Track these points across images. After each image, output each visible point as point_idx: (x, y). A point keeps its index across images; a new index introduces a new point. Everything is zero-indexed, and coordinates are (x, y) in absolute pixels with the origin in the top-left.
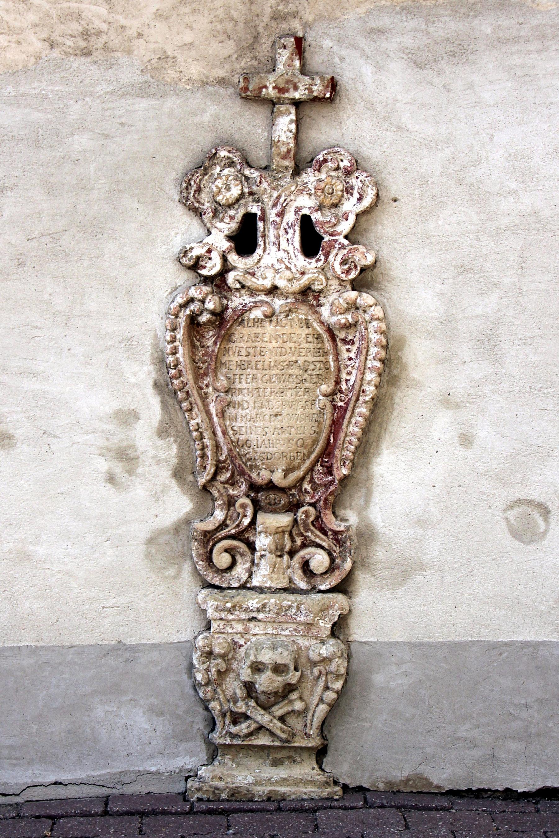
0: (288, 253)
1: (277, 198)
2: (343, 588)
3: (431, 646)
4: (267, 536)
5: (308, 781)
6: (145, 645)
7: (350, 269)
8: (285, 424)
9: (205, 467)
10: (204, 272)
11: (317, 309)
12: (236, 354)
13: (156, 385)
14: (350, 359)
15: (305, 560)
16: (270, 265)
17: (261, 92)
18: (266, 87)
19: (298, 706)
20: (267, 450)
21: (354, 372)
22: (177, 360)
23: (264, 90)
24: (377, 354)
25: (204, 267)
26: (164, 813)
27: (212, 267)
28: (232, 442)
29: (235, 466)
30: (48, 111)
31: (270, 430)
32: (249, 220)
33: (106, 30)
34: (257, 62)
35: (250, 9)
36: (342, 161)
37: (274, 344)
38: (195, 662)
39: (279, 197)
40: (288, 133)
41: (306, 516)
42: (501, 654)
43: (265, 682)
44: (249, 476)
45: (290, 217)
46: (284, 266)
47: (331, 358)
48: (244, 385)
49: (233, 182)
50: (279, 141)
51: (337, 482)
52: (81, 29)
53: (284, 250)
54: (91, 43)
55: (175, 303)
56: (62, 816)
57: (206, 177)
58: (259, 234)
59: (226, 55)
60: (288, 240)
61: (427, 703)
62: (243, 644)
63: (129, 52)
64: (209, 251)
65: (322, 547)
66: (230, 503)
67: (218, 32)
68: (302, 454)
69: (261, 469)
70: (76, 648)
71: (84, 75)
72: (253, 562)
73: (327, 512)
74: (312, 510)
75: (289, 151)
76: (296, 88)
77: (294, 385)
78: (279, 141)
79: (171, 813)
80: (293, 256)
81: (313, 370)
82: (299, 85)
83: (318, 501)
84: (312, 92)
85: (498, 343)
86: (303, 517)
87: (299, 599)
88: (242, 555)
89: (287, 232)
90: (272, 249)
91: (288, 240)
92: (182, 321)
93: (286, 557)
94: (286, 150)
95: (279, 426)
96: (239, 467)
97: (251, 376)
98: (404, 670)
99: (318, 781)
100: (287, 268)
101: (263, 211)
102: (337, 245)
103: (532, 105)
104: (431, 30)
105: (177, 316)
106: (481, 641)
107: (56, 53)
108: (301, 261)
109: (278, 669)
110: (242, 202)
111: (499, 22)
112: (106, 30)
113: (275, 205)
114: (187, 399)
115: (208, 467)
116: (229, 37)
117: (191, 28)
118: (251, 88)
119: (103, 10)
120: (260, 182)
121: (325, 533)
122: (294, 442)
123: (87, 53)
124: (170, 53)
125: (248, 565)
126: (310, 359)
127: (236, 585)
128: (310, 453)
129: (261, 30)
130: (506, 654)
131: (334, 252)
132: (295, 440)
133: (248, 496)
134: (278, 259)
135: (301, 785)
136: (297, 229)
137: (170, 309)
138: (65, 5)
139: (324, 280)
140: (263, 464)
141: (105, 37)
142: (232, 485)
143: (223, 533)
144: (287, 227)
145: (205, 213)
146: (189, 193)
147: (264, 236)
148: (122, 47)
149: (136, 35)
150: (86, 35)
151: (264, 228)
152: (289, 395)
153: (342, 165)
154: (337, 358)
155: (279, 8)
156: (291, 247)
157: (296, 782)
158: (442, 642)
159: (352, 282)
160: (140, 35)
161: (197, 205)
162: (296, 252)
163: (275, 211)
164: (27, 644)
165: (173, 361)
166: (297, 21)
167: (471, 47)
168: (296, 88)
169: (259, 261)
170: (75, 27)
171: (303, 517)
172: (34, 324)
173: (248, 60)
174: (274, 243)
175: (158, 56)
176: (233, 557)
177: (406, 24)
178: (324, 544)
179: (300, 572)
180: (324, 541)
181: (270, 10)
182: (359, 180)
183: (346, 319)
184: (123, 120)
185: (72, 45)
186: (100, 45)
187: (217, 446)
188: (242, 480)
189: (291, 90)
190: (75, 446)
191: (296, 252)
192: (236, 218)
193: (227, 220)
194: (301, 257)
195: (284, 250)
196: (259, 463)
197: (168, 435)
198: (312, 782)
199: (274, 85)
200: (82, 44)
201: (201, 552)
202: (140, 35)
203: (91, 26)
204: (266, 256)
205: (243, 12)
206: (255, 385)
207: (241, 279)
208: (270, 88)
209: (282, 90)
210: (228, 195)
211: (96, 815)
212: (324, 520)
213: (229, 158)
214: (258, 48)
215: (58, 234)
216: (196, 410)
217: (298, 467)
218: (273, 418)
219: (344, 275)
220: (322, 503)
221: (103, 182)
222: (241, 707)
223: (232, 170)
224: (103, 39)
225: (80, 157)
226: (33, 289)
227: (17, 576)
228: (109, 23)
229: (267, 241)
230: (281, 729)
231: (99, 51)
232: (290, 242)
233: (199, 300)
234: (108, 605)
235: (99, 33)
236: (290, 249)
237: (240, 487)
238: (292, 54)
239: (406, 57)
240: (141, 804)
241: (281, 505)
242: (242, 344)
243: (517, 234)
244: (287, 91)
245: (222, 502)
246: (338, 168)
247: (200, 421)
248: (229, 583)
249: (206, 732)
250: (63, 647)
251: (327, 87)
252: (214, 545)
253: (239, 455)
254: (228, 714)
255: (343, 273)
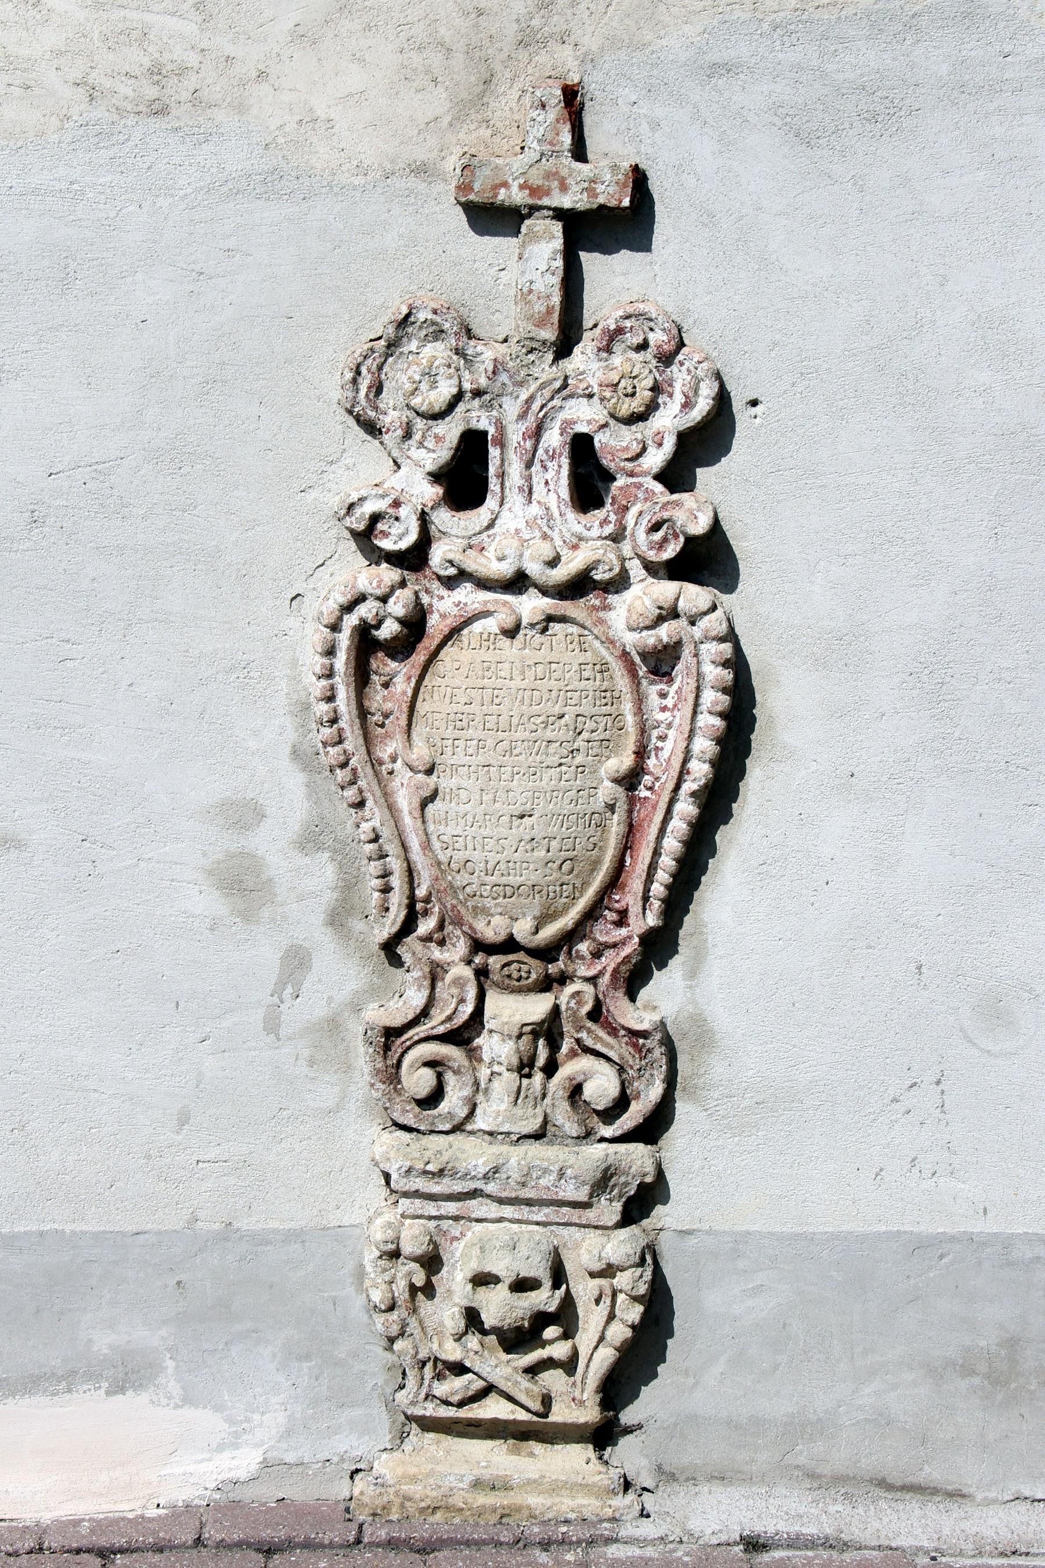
0: (547, 509)
1: (527, 401)
2: (653, 1128)
3: (810, 1238)
4: (503, 1040)
5: (576, 1484)
6: (275, 1231)
7: (665, 540)
8: (538, 833)
9: (387, 909)
10: (386, 544)
11: (601, 614)
12: (447, 700)
13: (296, 753)
14: (664, 709)
15: (575, 1082)
16: (513, 532)
17: (496, 195)
18: (505, 185)
19: (560, 1350)
20: (504, 880)
21: (671, 733)
22: (335, 711)
23: (503, 191)
24: (716, 703)
25: (385, 534)
26: (308, 1545)
27: (399, 537)
28: (439, 863)
29: (445, 907)
30: (84, 224)
31: (510, 843)
32: (473, 447)
33: (196, 65)
34: (489, 132)
35: (476, 26)
36: (651, 329)
37: (517, 683)
38: (369, 1269)
39: (530, 400)
40: (548, 275)
41: (578, 1003)
42: (941, 1257)
43: (498, 1307)
44: (471, 927)
45: (554, 438)
46: (538, 534)
47: (627, 707)
48: (460, 758)
49: (442, 370)
50: (531, 291)
51: (637, 940)
52: (147, 63)
53: (539, 502)
54: (168, 91)
55: (331, 602)
56: (122, 1551)
57: (390, 359)
58: (492, 470)
59: (430, 116)
60: (547, 483)
61: (801, 1343)
62: (458, 1234)
63: (241, 108)
64: (396, 504)
65: (608, 1059)
66: (435, 974)
67: (415, 70)
68: (571, 887)
69: (492, 915)
70: (147, 1236)
71: (155, 155)
72: (477, 1084)
73: (617, 994)
74: (588, 989)
75: (549, 311)
76: (564, 188)
77: (555, 760)
78: (531, 291)
79: (322, 1546)
80: (556, 514)
81: (593, 731)
82: (569, 181)
83: (601, 973)
84: (596, 196)
85: (948, 679)
86: (572, 1004)
87: (561, 1157)
88: (457, 1072)
89: (545, 468)
90: (515, 499)
91: (547, 483)
92: (344, 639)
93: (538, 1077)
94: (543, 309)
95: (528, 837)
96: (452, 910)
97: (475, 742)
98: (759, 1283)
99: (594, 1485)
100: (545, 537)
101: (501, 427)
102: (640, 495)
103: (1024, 217)
104: (830, 67)
105: (335, 628)
106: (905, 1232)
107: (99, 112)
108: (574, 522)
109: (522, 1285)
110: (461, 408)
111: (964, 53)
112: (196, 65)
113: (523, 416)
114: (354, 783)
115: (393, 909)
116: (435, 80)
117: (362, 61)
118: (477, 186)
119: (190, 28)
120: (494, 373)
121: (613, 1031)
122: (555, 866)
123: (160, 111)
124: (321, 113)
125: (467, 1092)
126: (586, 708)
127: (447, 1127)
128: (585, 884)
129: (498, 67)
130: (950, 1257)
131: (634, 511)
132: (558, 862)
133: (469, 962)
134: (527, 520)
135: (563, 1492)
136: (565, 462)
137: (322, 613)
138: (117, 14)
139: (615, 562)
140: (496, 905)
141: (193, 79)
142: (442, 943)
143: (420, 1031)
144: (544, 457)
145: (389, 430)
146: (357, 391)
147: (502, 476)
148: (228, 100)
149: (255, 74)
150: (156, 72)
151: (503, 460)
152: (546, 779)
153: (652, 337)
154: (640, 708)
155: (533, 23)
156: (553, 496)
157: (556, 1488)
158: (832, 1234)
159: (669, 563)
160: (262, 75)
161: (372, 414)
162: (563, 507)
163: (522, 427)
164: (56, 1226)
165: (327, 712)
166: (567, 51)
167: (907, 102)
168: (564, 188)
169: (491, 525)
170: (137, 59)
171: (572, 1004)
172: (63, 635)
173: (472, 127)
174: (521, 489)
175: (299, 118)
176: (440, 1076)
177: (780, 56)
178: (611, 1054)
179: (565, 1105)
180: (612, 1048)
181: (516, 26)
182: (684, 368)
183: (658, 636)
184: (231, 243)
185: (131, 94)
186: (185, 95)
187: (410, 872)
188: (458, 932)
189: (556, 192)
190: (142, 864)
191: (563, 507)
192: (448, 439)
193: (430, 443)
194: (571, 515)
195: (539, 502)
196: (489, 903)
197: (320, 848)
198: (586, 1488)
199: (522, 181)
200: (152, 92)
201: (379, 1066)
202: (262, 75)
203: (167, 56)
204: (505, 514)
205: (463, 31)
206: (481, 759)
207: (457, 557)
208: (515, 189)
209: (535, 191)
210: (433, 396)
211: (183, 1546)
212: (611, 1009)
213: (433, 323)
214: (492, 104)
215: (107, 465)
216: (370, 803)
217: (566, 909)
218: (516, 822)
219: (652, 553)
220: (607, 977)
221: (192, 364)
222: (452, 1352)
223: (439, 345)
224: (191, 82)
225: (147, 316)
226: (60, 570)
227: (35, 1104)
228: (203, 50)
229: (507, 484)
230: (528, 1392)
231: (183, 108)
232: (552, 487)
233: (378, 598)
234: (207, 1157)
235: (182, 71)
236: (552, 501)
237: (454, 945)
238: (558, 121)
239: (779, 123)
240: (266, 1526)
241: (530, 980)
242: (457, 682)
243: (989, 469)
244: (548, 193)
245: (420, 974)
246: (643, 346)
247: (378, 825)
248: (433, 1124)
249: (389, 1390)
250: (123, 1234)
251: (625, 186)
252: (402, 1055)
253: (452, 887)
254: (429, 1366)
255: (651, 549)
